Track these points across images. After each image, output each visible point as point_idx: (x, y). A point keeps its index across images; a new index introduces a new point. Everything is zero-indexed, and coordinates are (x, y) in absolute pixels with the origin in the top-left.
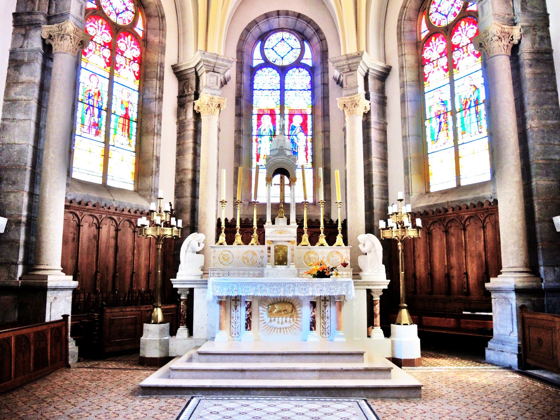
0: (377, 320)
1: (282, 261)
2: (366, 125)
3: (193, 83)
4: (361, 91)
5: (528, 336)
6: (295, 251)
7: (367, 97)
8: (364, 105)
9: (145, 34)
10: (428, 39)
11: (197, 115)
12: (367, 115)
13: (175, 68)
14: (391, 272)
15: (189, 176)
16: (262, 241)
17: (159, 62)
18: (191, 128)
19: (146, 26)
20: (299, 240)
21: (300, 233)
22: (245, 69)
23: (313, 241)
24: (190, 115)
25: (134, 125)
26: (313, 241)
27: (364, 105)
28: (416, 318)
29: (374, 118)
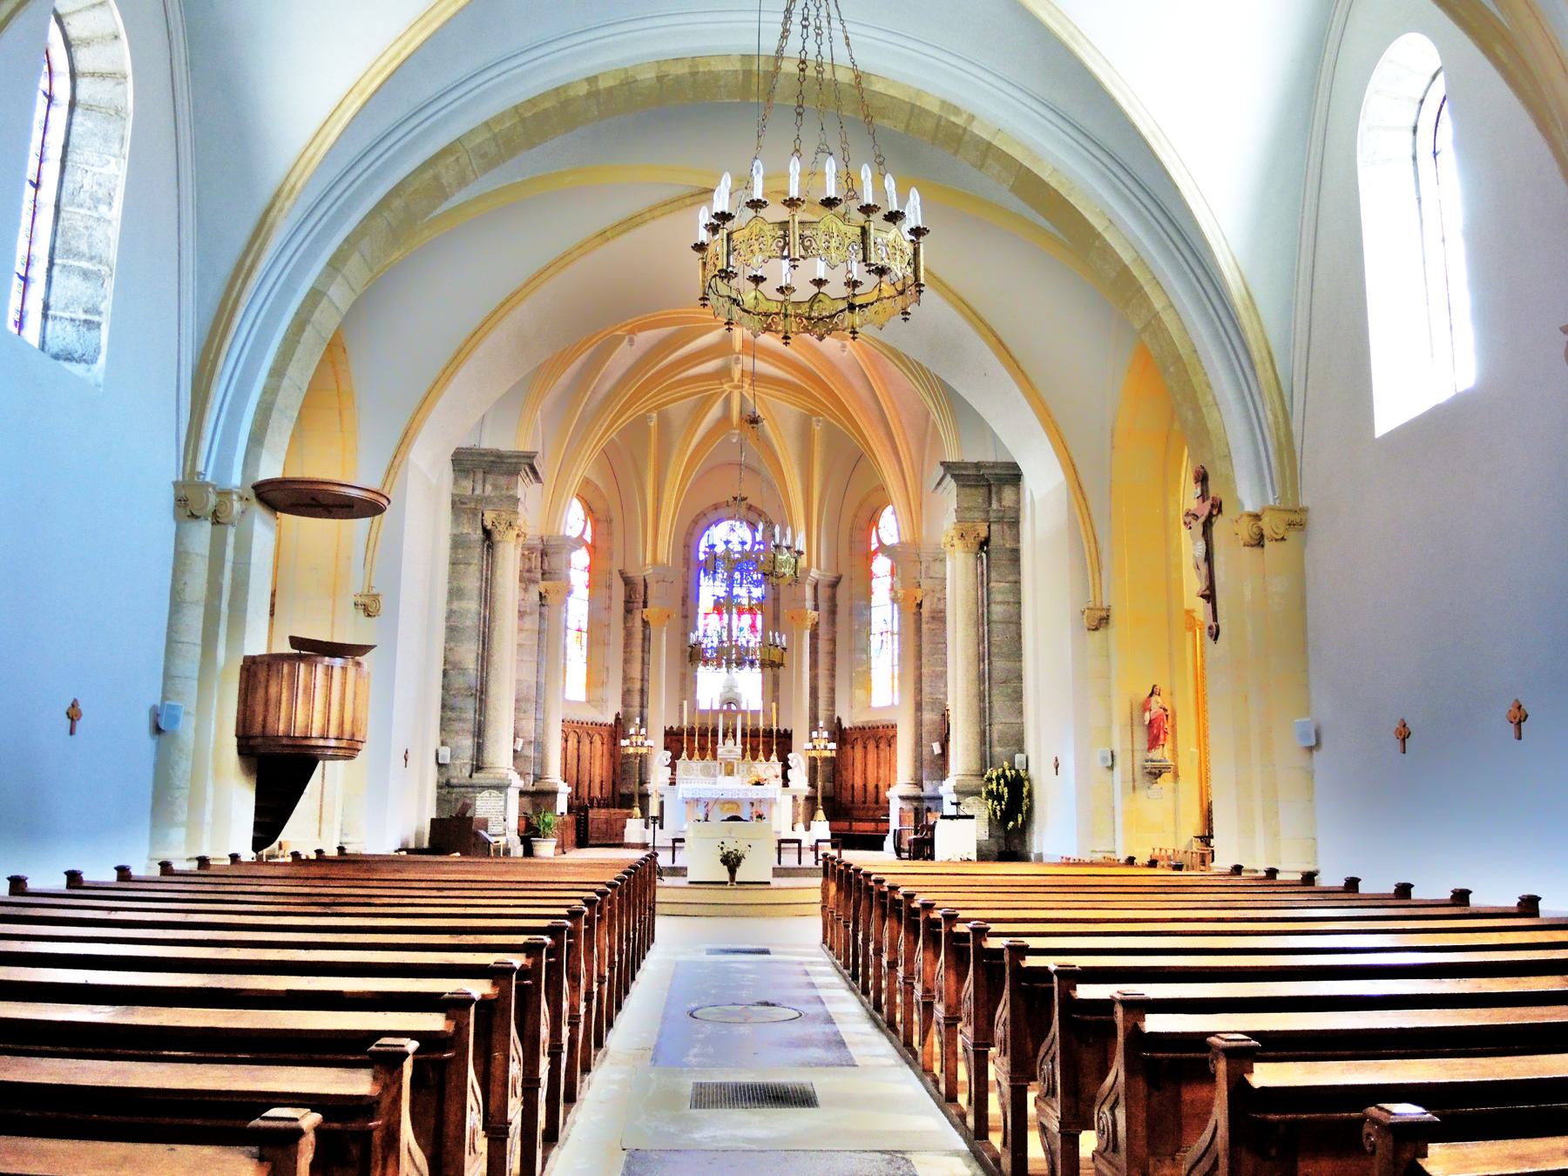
0: (801, 818)
1: (730, 773)
2: (814, 636)
3: (641, 589)
4: (809, 604)
5: (260, 719)
6: (740, 767)
7: (816, 608)
8: (812, 615)
9: (593, 539)
10: (876, 552)
11: (645, 623)
12: (815, 626)
13: (621, 573)
14: (812, 784)
15: (638, 685)
16: (715, 757)
17: (697, 726)
18: (638, 637)
19: (594, 531)
20: (743, 757)
21: (744, 750)
22: (693, 566)
23: (754, 758)
24: (638, 624)
25: (585, 636)
26: (754, 758)
27: (812, 615)
28: (830, 817)
29: (823, 631)
